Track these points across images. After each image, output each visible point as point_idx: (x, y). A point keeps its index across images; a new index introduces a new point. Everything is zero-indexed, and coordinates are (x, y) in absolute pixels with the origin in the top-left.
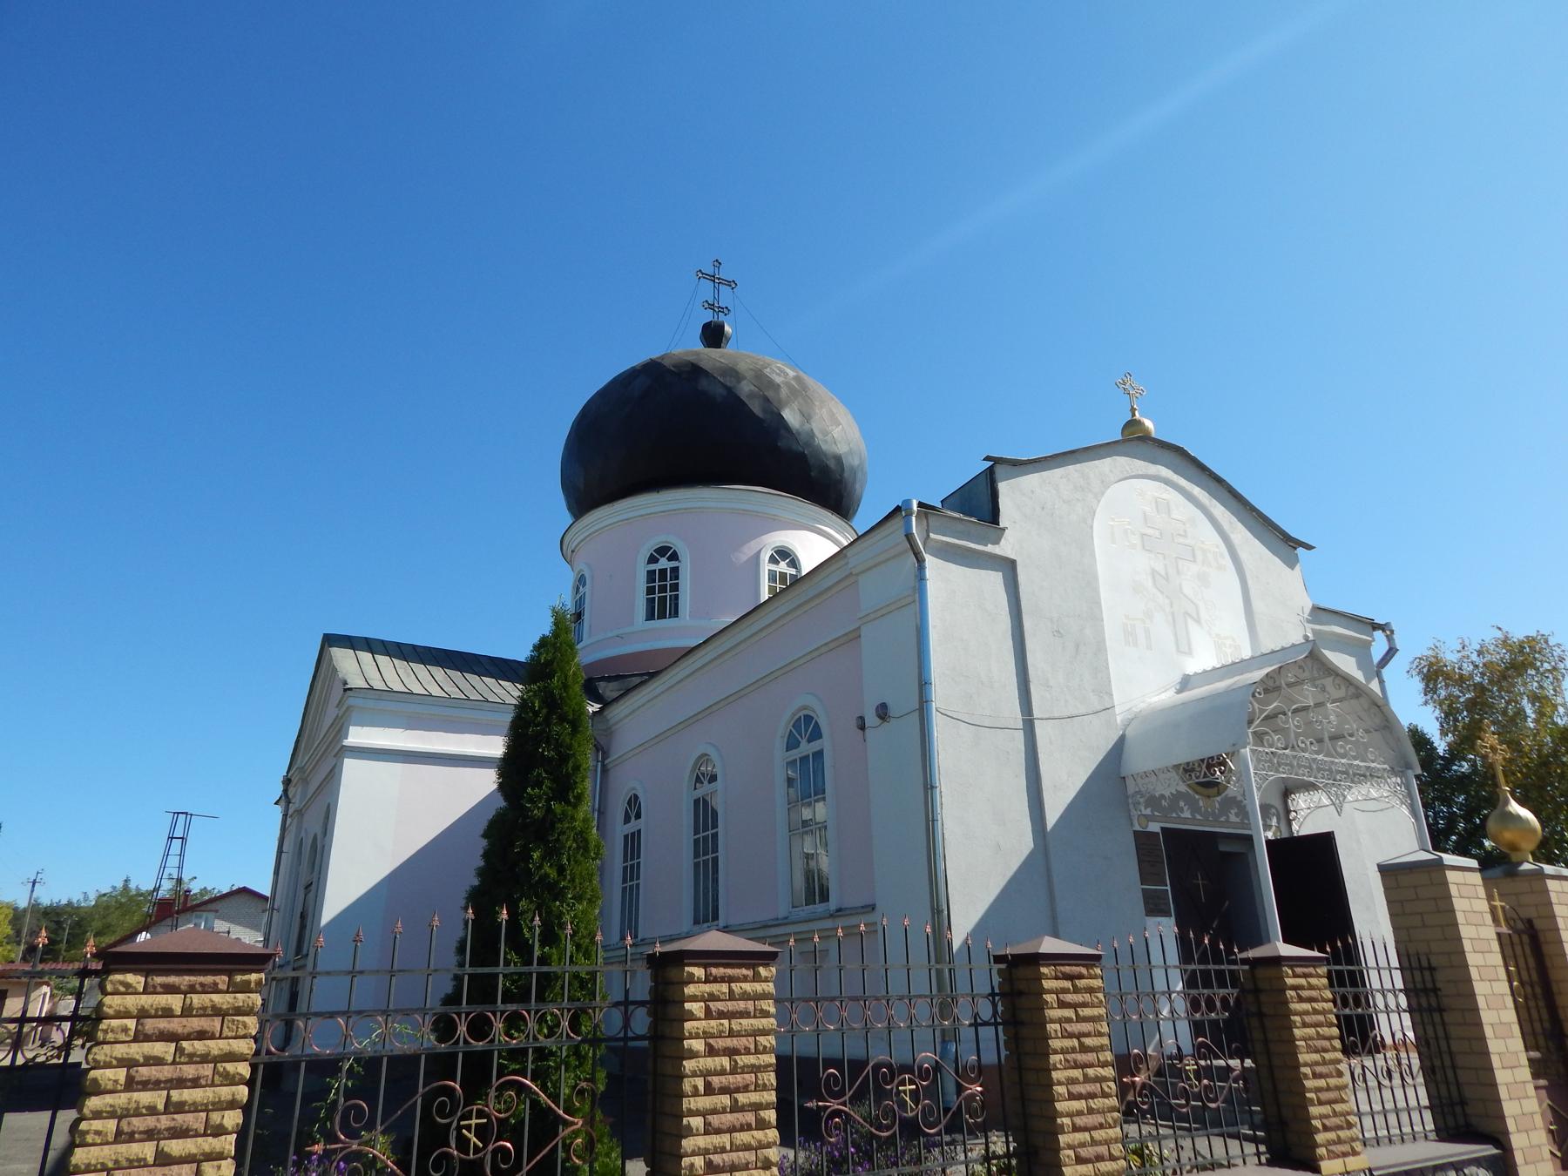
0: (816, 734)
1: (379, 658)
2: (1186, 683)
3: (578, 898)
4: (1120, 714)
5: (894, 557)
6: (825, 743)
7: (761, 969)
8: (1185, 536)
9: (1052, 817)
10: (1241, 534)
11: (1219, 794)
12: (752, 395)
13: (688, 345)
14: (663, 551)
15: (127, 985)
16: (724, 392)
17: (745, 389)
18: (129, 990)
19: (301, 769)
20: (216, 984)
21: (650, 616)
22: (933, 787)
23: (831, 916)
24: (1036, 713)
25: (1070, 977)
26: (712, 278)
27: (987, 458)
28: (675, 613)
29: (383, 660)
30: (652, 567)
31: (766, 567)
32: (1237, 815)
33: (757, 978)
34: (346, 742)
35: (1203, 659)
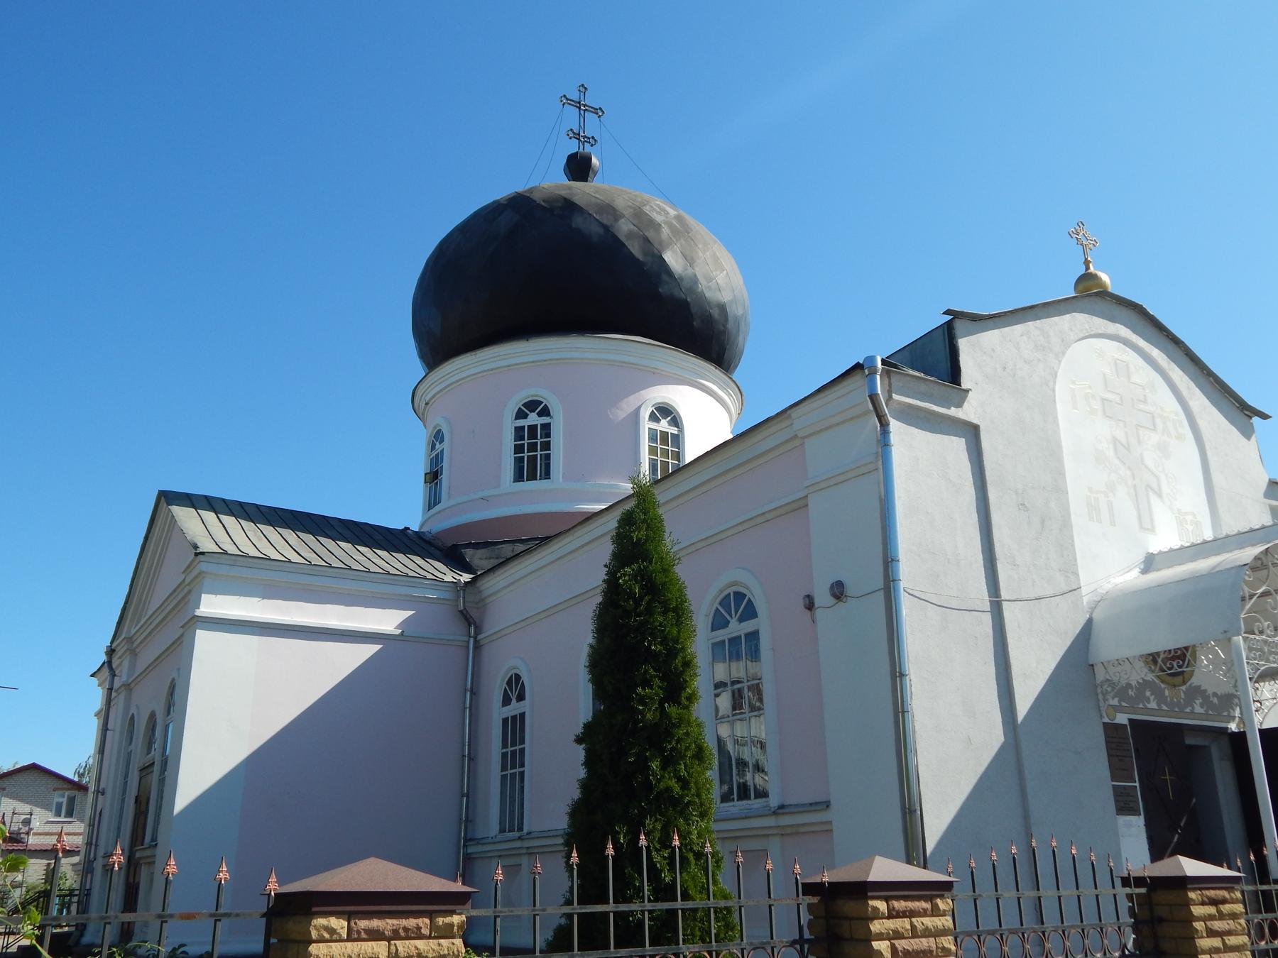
0: (750, 613)
1: (222, 517)
2: (1150, 563)
3: (703, 815)
4: (1087, 595)
5: (852, 419)
6: (762, 624)
7: (939, 901)
8: (1145, 402)
9: (1023, 707)
10: (1199, 401)
11: (1184, 683)
12: (630, 235)
13: (550, 178)
14: (532, 405)
15: (332, 931)
16: (601, 231)
17: (624, 228)
18: (333, 937)
19: (130, 640)
20: (419, 928)
21: (519, 477)
22: (902, 675)
23: (774, 813)
24: (1004, 594)
25: (1214, 902)
26: (578, 104)
27: (947, 312)
28: (547, 474)
29: (229, 520)
30: (521, 423)
31: (646, 425)
32: (1202, 706)
33: (935, 912)
34: (198, 612)
35: (1166, 538)
